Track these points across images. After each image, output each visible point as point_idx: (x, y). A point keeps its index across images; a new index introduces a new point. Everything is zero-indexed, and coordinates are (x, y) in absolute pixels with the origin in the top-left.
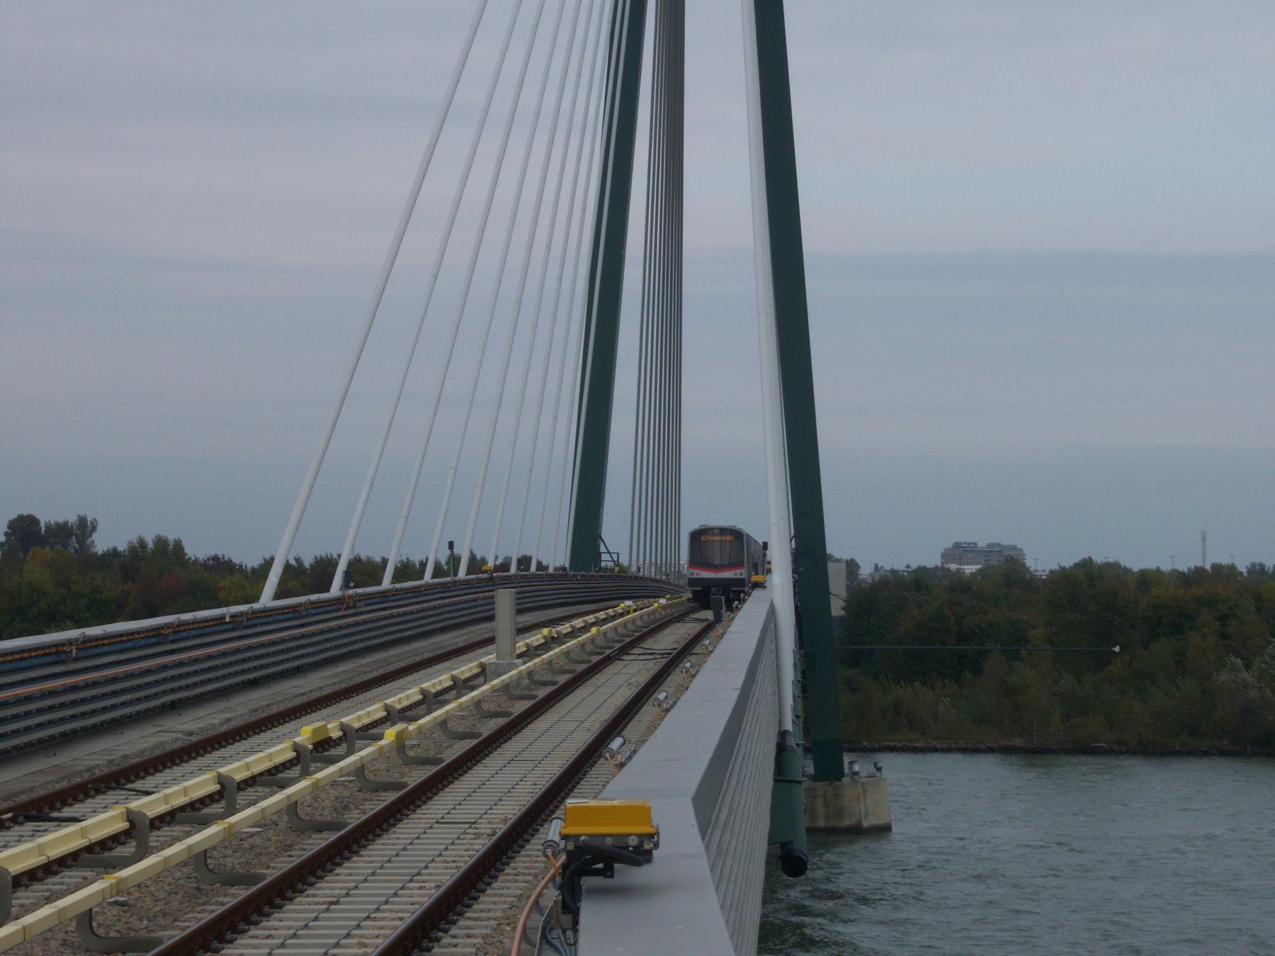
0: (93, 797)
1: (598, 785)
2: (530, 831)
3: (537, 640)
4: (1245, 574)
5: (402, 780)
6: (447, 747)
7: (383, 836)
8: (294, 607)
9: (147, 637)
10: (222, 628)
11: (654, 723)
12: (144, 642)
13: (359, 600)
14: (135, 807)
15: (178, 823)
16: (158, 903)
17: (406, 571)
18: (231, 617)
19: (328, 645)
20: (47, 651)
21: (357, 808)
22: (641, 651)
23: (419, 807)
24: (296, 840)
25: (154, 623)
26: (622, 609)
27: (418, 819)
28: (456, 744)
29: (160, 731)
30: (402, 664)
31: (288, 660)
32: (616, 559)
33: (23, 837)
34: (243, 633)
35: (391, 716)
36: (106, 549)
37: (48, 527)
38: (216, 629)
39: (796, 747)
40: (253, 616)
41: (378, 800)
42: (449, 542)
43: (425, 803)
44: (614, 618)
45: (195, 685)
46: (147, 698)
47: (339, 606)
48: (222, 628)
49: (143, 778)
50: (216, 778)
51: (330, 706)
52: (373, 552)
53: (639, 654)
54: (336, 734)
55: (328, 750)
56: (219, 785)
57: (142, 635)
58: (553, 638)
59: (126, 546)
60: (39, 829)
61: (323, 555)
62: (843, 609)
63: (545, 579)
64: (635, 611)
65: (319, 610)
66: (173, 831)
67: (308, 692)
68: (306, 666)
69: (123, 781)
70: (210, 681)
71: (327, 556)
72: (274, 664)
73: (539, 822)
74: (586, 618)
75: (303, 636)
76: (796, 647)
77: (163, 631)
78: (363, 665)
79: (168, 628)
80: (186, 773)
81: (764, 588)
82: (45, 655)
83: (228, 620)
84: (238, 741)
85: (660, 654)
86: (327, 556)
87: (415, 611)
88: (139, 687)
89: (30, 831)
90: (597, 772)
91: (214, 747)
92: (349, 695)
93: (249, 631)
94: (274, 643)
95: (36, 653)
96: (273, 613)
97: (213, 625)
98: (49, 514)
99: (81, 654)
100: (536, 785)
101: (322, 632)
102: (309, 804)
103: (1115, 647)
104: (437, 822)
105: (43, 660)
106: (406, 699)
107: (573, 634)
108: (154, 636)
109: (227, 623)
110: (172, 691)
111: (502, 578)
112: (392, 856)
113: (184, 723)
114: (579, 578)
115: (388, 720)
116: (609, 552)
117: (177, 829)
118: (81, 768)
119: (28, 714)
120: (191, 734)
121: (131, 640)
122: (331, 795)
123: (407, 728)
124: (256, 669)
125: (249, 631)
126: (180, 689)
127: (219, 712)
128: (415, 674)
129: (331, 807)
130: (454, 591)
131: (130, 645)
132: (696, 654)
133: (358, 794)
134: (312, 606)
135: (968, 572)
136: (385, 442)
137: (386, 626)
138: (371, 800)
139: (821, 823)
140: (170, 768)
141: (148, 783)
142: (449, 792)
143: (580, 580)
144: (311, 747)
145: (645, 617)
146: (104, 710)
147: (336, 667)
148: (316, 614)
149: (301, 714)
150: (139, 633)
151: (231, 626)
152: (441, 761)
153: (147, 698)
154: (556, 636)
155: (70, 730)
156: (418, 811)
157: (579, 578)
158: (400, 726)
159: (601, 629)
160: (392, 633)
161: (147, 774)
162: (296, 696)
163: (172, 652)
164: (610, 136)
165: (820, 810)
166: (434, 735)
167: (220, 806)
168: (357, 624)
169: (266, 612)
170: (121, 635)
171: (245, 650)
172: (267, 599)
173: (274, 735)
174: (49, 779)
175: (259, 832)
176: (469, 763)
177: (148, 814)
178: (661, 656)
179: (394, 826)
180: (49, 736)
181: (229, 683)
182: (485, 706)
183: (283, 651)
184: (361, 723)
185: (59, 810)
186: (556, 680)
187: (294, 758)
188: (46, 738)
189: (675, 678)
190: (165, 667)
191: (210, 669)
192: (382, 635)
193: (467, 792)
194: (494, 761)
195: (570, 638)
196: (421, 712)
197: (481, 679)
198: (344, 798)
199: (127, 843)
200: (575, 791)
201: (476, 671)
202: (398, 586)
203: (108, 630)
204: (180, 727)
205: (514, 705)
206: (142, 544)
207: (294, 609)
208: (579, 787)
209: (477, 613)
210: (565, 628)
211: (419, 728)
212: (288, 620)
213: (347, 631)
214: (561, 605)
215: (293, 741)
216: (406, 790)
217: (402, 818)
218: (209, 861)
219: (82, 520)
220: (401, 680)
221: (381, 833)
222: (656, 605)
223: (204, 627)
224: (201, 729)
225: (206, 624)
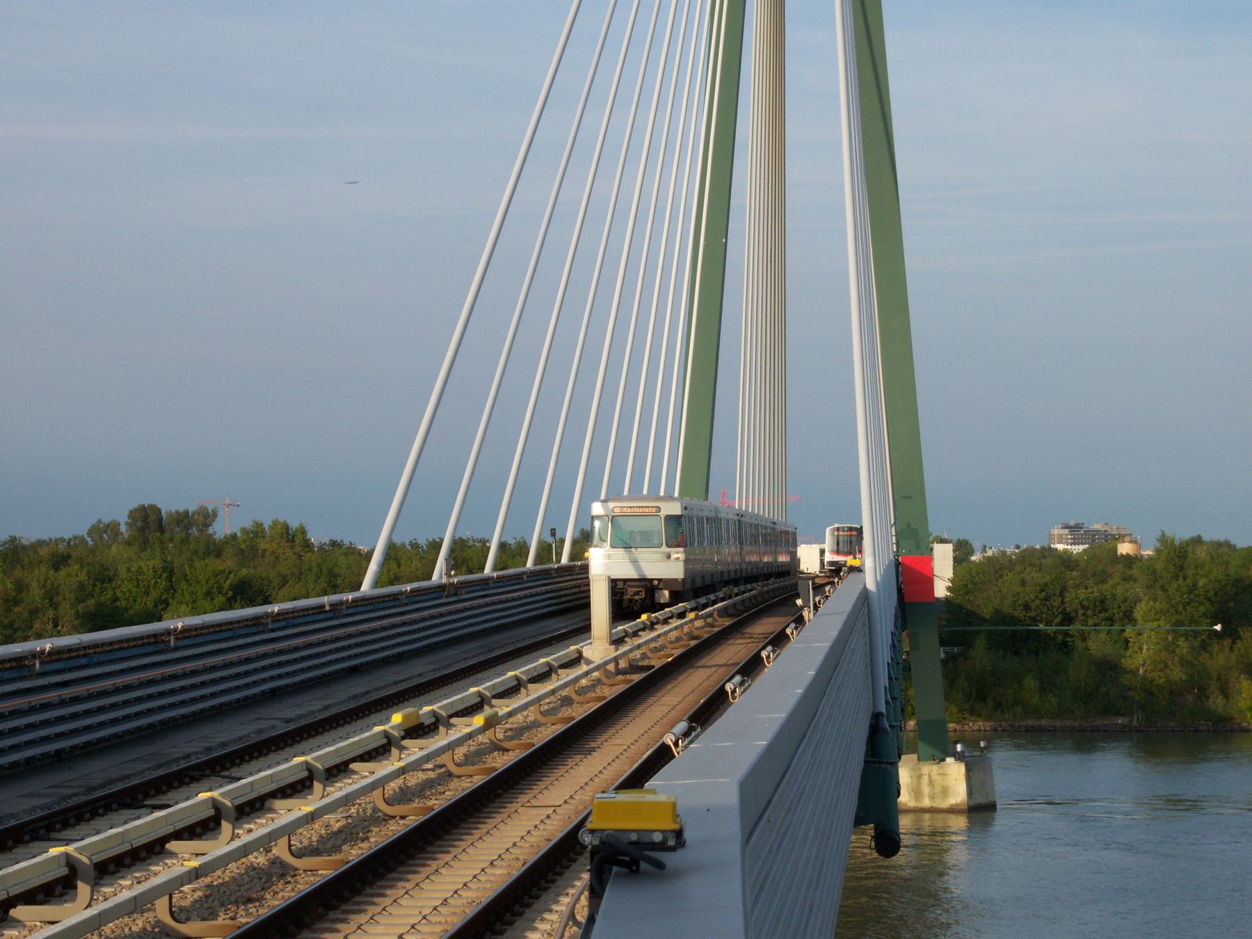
0: (188, 784)
8: (394, 595)
9: (247, 626)
10: (321, 616)
16: (241, 888)
20: (146, 641)
31: (388, 647)
37: (170, 514)
39: (889, 728)
40: (353, 604)
42: (552, 530)
46: (247, 686)
48: (321, 616)
56: (307, 772)
57: (242, 624)
62: (949, 589)
64: (737, 595)
68: (407, 653)
69: (218, 768)
70: (310, 668)
76: (896, 627)
77: (262, 621)
82: (144, 645)
83: (327, 608)
88: (238, 676)
91: (271, 748)
95: (102, 649)
96: (373, 601)
97: (314, 614)
98: (169, 504)
99: (181, 643)
103: (1216, 625)
105: (142, 650)
108: (254, 625)
109: (327, 612)
110: (272, 678)
118: (179, 755)
119: (127, 703)
120: (288, 721)
121: (230, 630)
126: (280, 676)
131: (84, 661)
134: (413, 594)
135: (1075, 552)
139: (926, 803)
145: (747, 601)
146: (88, 729)
147: (280, 702)
148: (417, 602)
150: (238, 622)
151: (330, 615)
153: (247, 686)
155: (159, 721)
159: (700, 614)
163: (273, 640)
164: (722, 12)
165: (926, 790)
169: (486, 581)
170: (220, 625)
172: (439, 573)
174: (146, 766)
180: (25, 758)
183: (383, 639)
187: (478, 703)
188: (208, 708)
190: (265, 656)
191: (310, 657)
202: (572, 563)
203: (421, 585)
204: (279, 715)
207: (395, 597)
212: (389, 608)
216: (575, 721)
218: (174, 909)
223: (304, 616)
225: (306, 613)
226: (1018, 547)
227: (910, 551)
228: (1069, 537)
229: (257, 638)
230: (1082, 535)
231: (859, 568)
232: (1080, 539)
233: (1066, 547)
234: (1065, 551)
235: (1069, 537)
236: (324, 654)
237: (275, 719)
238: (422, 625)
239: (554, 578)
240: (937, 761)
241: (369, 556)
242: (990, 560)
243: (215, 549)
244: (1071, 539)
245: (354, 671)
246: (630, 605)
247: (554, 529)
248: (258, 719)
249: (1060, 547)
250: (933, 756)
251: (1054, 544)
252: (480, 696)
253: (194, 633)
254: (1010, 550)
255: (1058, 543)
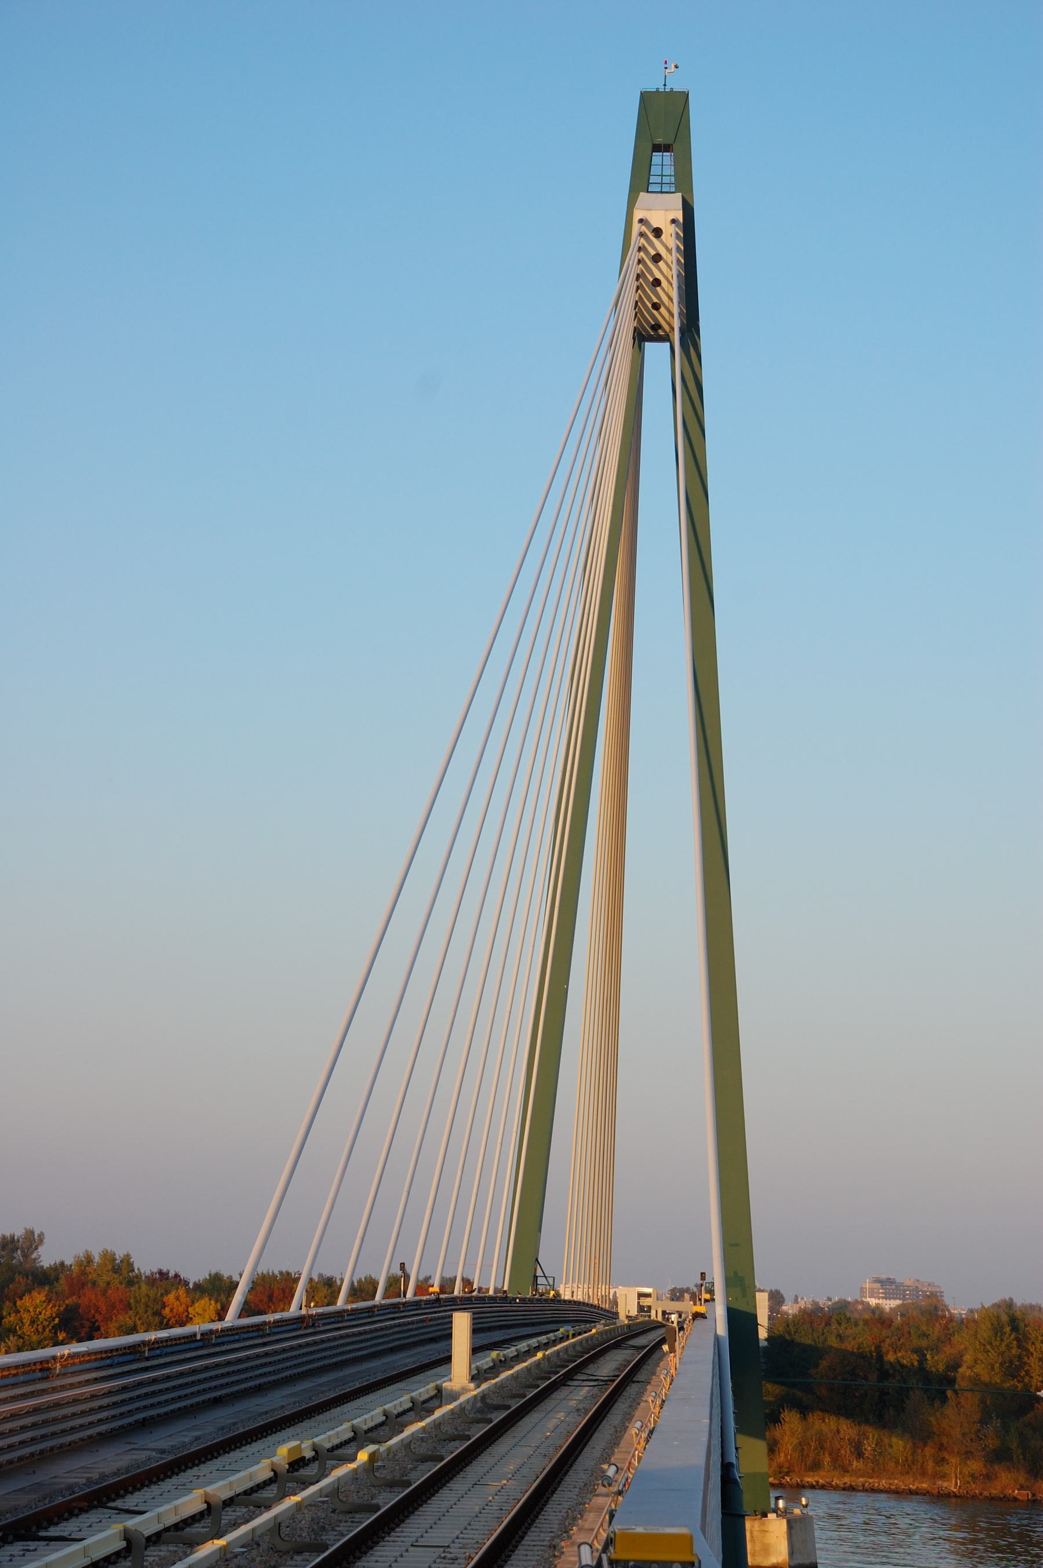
0: (77, 1516)
1: (561, 1512)
2: (503, 1557)
3: (487, 1363)
4: (191, 1286)
5: (373, 1502)
6: (411, 1469)
7: (363, 1558)
8: (258, 1325)
10: (193, 1345)
11: (607, 1450)
12: (121, 1359)
13: (318, 1320)
14: (132, 1525)
15: (164, 1543)
17: (363, 1289)
18: (202, 1335)
19: (288, 1364)
21: (334, 1530)
22: (585, 1377)
23: (393, 1529)
24: (279, 1561)
25: (131, 1341)
26: (562, 1333)
27: (394, 1541)
28: (420, 1466)
29: (133, 1449)
30: (358, 1385)
32: (551, 1283)
33: (14, 1556)
34: (212, 1351)
35: (358, 1438)
36: (52, 1263)
38: (187, 1346)
41: (352, 1522)
42: (401, 1264)
43: (398, 1526)
44: (554, 1342)
45: (167, 1402)
47: (299, 1325)
48: (193, 1345)
49: (123, 1497)
50: (203, 1496)
51: (293, 1425)
52: (274, 1266)
53: (583, 1380)
54: (309, 1454)
55: (297, 1470)
58: (501, 1361)
59: (73, 1260)
60: (28, 1548)
61: (265, 1272)
63: (474, 1302)
64: (574, 1336)
65: (280, 1329)
66: (160, 1551)
67: (270, 1410)
71: (268, 1273)
72: (238, 1382)
73: (511, 1548)
74: (539, 1338)
75: (266, 1354)
78: (320, 1385)
79: (144, 1345)
80: (94, 1523)
81: (704, 1318)
84: (210, 1460)
85: (602, 1381)
86: (268, 1273)
87: (264, 1354)
89: (20, 1551)
90: (558, 1499)
92: (311, 1414)
93: (217, 1349)
94: (239, 1361)
96: (240, 1331)
100: (502, 1510)
101: (284, 1350)
102: (287, 1524)
104: (412, 1545)
106: (370, 1420)
107: (519, 1358)
111: (447, 1300)
112: (418, 1537)
113: (156, 1441)
114: (518, 1301)
115: (317, 1460)
116: (546, 1277)
117: (241, 1511)
118: (62, 1486)
120: (163, 1451)
122: (306, 1515)
123: (379, 1449)
124: (222, 1386)
125: (217, 1349)
127: (188, 1430)
128: (371, 1394)
129: (309, 1528)
130: (403, 1311)
132: (638, 1382)
133: (332, 1515)
136: (409, 1193)
137: (342, 1345)
138: (346, 1522)
140: (147, 1486)
141: (131, 1501)
142: (419, 1515)
143: (518, 1303)
144: (287, 1466)
149: (294, 1421)
151: (200, 1344)
152: (377, 1508)
154: (503, 1359)
156: (393, 1534)
157: (518, 1301)
158: (372, 1448)
159: (547, 1353)
160: (350, 1351)
161: (127, 1492)
162: (260, 1415)
166: (397, 1458)
167: (201, 1525)
168: (315, 1343)
169: (340, 1314)
171: (213, 1367)
173: (243, 1455)
175: (243, 1553)
176: (415, 1504)
177: (144, 1533)
178: (604, 1383)
179: (372, 1548)
181: (208, 1397)
182: (444, 1428)
184: (331, 1443)
185: (46, 1529)
186: (507, 1404)
189: (620, 1407)
191: (181, 1387)
192: (334, 1356)
193: (437, 1516)
194: (458, 1485)
195: (516, 1361)
196: (411, 1419)
197: (436, 1402)
198: (319, 1518)
199: (117, 1562)
200: (540, 1517)
201: (433, 1393)
203: (172, 1334)
204: (152, 1445)
205: (470, 1428)
206: (89, 1260)
207: (258, 1327)
208: (543, 1513)
209: (424, 1334)
210: (511, 1352)
211: (389, 1450)
212: (252, 1338)
213: (305, 1350)
214: (501, 1327)
215: (271, 1461)
217: (354, 1561)
219: (30, 1233)
220: (358, 1400)
221: (360, 1555)
222: (594, 1331)
224: (173, 1446)
226: (829, 1299)
227: (737, 1299)
228: (881, 1291)
229: (134, 1366)
230: (893, 1290)
231: (704, 1314)
232: (891, 1294)
233: (877, 1301)
234: (878, 1306)
235: (881, 1291)
236: (193, 1383)
237: (148, 1449)
238: (362, 1337)
239: (458, 1305)
240: (759, 1517)
241: (234, 1286)
242: (803, 1312)
243: (44, 1278)
244: (883, 1293)
245: (217, 1402)
246: (680, 1320)
247: (404, 1264)
248: (133, 1449)
249: (873, 1302)
250: (755, 1511)
251: (866, 1297)
252: (384, 1415)
253: (251, 1329)
254: (822, 1302)
255: (869, 1297)
